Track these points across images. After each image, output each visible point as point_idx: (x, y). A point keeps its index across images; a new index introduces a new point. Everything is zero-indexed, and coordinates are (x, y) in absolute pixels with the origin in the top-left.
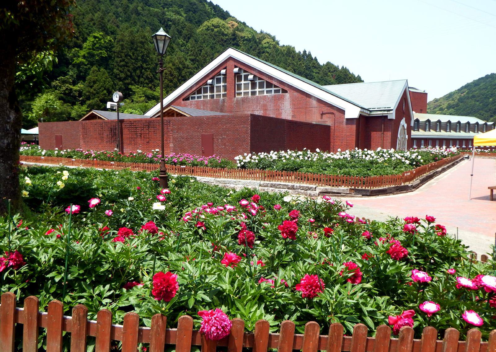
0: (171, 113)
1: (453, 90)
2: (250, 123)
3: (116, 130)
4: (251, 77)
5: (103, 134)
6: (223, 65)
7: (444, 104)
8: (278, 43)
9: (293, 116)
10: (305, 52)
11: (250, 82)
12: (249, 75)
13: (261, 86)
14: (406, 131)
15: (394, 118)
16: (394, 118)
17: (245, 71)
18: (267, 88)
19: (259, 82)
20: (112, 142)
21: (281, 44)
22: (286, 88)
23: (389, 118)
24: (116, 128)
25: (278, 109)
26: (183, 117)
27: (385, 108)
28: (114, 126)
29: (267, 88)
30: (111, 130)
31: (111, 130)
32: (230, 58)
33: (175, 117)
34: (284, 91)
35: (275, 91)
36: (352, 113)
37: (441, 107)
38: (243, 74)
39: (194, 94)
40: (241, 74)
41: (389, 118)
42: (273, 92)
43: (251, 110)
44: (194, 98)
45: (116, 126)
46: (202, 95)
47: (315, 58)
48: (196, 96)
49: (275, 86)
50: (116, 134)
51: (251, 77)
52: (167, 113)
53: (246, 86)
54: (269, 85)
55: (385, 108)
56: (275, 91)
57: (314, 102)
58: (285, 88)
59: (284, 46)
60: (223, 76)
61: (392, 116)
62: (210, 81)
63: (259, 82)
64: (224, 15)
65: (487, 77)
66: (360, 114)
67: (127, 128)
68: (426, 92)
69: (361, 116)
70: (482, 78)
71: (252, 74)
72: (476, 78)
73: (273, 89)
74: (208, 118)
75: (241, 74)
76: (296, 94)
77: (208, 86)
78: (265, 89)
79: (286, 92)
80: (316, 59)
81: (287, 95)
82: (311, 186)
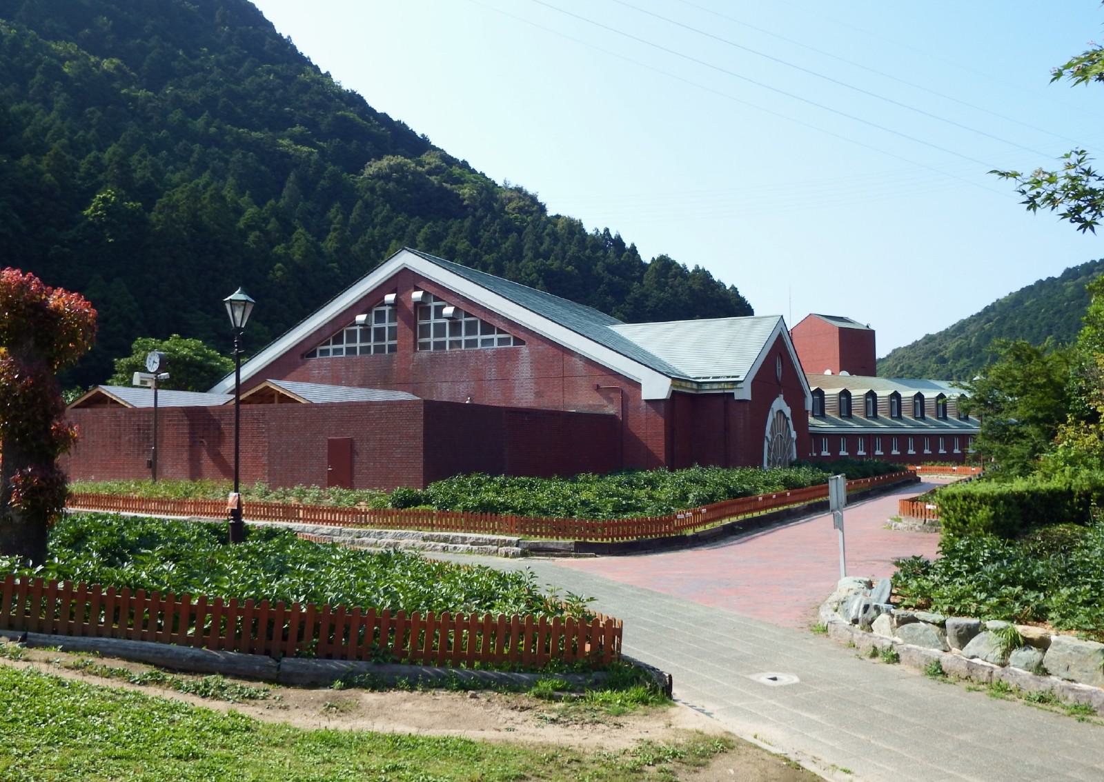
0: (268, 396)
1: (966, 316)
2: (422, 413)
3: (149, 429)
4: (448, 311)
5: (119, 438)
6: (391, 284)
7: (946, 348)
8: (542, 209)
9: (539, 394)
10: (607, 230)
11: (447, 322)
12: (444, 306)
13: (471, 329)
14: (790, 422)
15: (749, 397)
16: (749, 397)
17: (437, 299)
18: (482, 333)
19: (466, 322)
20: (139, 455)
21: (551, 212)
22: (522, 336)
23: (737, 397)
24: (149, 426)
25: (505, 380)
26: (295, 404)
27: (728, 377)
28: (144, 421)
29: (482, 333)
30: (139, 429)
31: (139, 429)
32: (405, 272)
33: (276, 404)
34: (518, 341)
35: (501, 341)
36: (656, 388)
37: (942, 354)
38: (433, 304)
39: (328, 343)
40: (429, 304)
41: (737, 397)
42: (496, 342)
43: (450, 380)
44: (326, 352)
45: (149, 421)
46: (344, 346)
47: (633, 245)
48: (331, 347)
49: (500, 332)
50: (148, 438)
51: (448, 311)
52: (256, 396)
53: (440, 330)
54: (488, 328)
55: (728, 377)
56: (501, 341)
57: (580, 364)
58: (522, 335)
59: (558, 217)
60: (390, 308)
61: (744, 393)
62: (361, 318)
63: (466, 322)
64: (422, 145)
65: (1040, 283)
66: (673, 391)
67: (174, 425)
68: (872, 327)
69: (674, 394)
70: (1030, 288)
71: (450, 305)
72: (1016, 288)
73: (496, 336)
74: (341, 406)
75: (429, 304)
76: (542, 347)
77: (358, 328)
78: (479, 337)
79: (523, 343)
80: (633, 248)
81: (524, 350)
82: (508, 538)
